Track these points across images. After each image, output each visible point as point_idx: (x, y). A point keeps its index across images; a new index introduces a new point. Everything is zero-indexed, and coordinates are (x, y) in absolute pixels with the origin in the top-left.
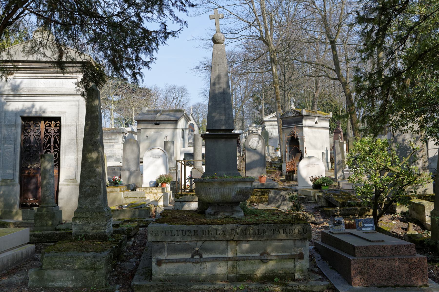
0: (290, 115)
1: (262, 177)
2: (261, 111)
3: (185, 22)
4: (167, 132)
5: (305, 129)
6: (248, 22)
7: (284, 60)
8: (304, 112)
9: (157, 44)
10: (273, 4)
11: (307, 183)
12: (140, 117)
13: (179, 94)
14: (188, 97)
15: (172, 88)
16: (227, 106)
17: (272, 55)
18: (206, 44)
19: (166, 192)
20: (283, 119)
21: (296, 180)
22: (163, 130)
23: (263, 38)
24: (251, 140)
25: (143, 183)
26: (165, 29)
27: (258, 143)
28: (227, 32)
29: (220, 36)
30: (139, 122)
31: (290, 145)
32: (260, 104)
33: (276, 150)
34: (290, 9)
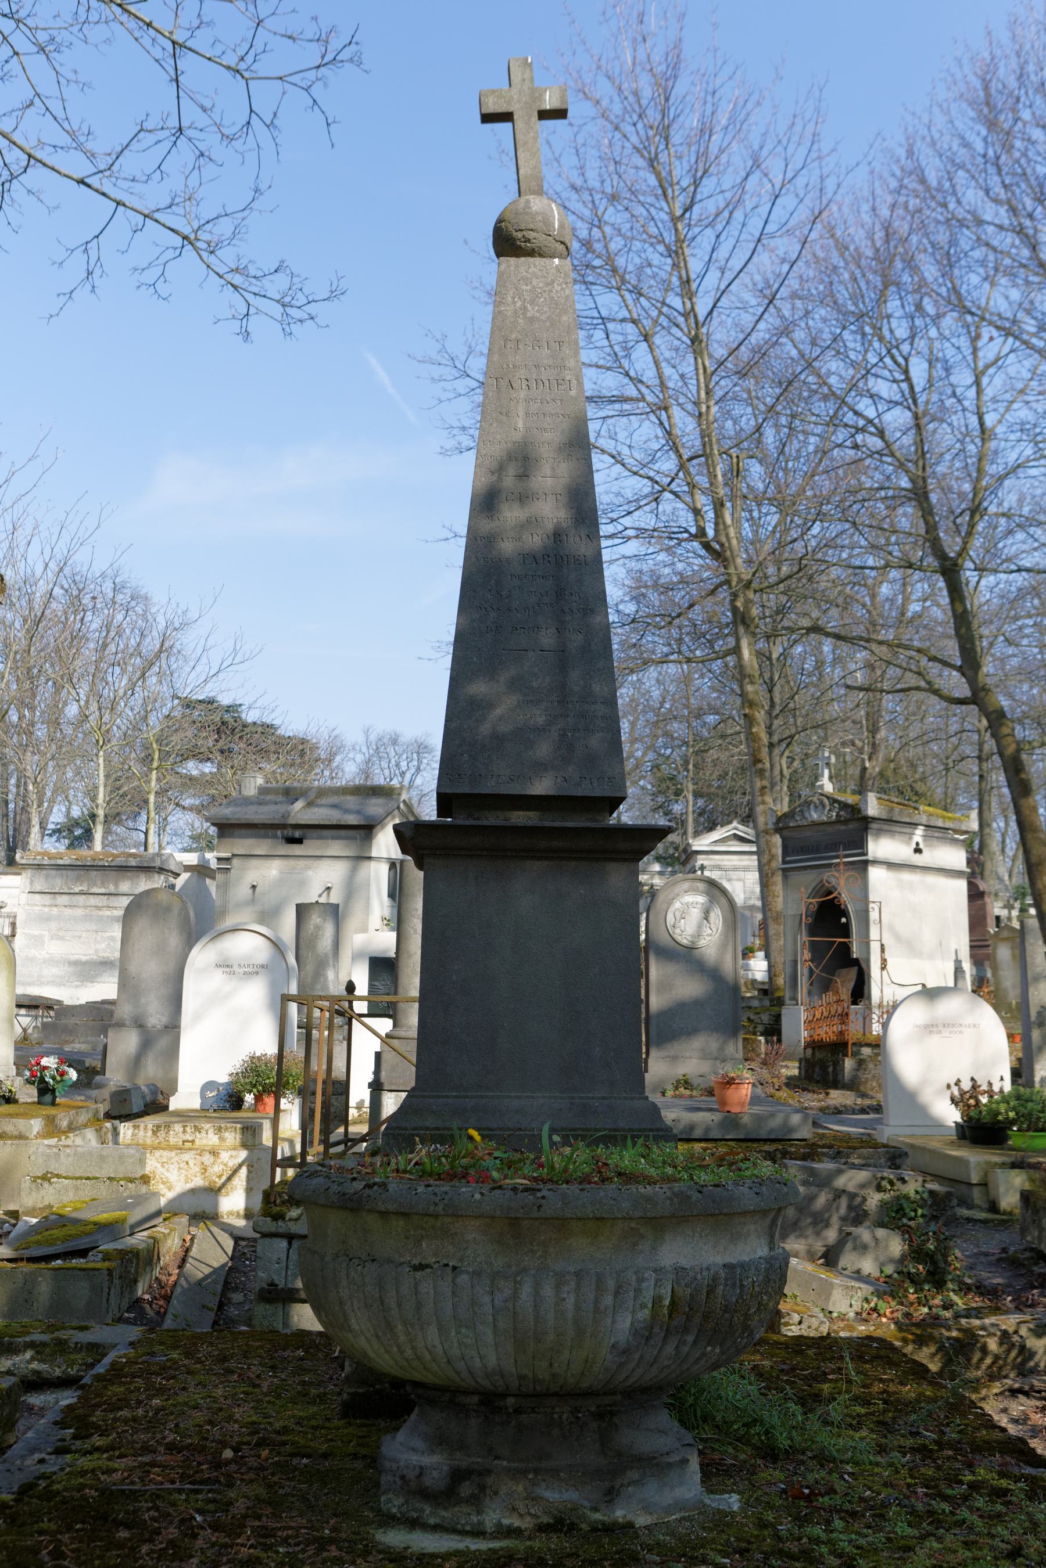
0: (815, 816)
1: (730, 1082)
4: (323, 875)
5: (875, 874)
8: (873, 807)
11: (922, 1111)
13: (409, 760)
15: (385, 740)
20: (786, 833)
24: (677, 905)
25: (174, 1090)
27: (706, 918)
31: (812, 932)
32: (678, 793)
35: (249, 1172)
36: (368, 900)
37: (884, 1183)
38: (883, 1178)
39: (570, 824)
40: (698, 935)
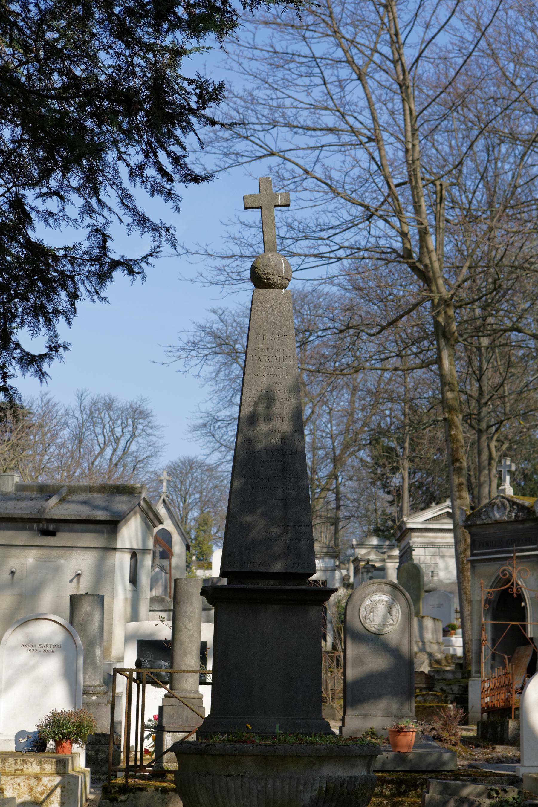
0: (497, 516)
1: (399, 731)
2: (398, 494)
3: (167, 230)
4: (77, 563)
6: (362, 205)
7: (479, 331)
9: (73, 296)
10: (446, 149)
13: (124, 426)
14: (153, 439)
15: (100, 405)
16: (293, 493)
17: (438, 313)
18: (220, 270)
19: (70, 771)
20: (474, 530)
21: (515, 742)
22: (68, 552)
23: (411, 257)
24: (368, 602)
26: (104, 248)
28: (292, 234)
29: (276, 262)
32: (395, 470)
33: (448, 631)
34: (499, 165)
35: (62, 791)
36: (113, 584)
37: (493, 793)
38: (492, 790)
39: (289, 587)
40: (384, 624)
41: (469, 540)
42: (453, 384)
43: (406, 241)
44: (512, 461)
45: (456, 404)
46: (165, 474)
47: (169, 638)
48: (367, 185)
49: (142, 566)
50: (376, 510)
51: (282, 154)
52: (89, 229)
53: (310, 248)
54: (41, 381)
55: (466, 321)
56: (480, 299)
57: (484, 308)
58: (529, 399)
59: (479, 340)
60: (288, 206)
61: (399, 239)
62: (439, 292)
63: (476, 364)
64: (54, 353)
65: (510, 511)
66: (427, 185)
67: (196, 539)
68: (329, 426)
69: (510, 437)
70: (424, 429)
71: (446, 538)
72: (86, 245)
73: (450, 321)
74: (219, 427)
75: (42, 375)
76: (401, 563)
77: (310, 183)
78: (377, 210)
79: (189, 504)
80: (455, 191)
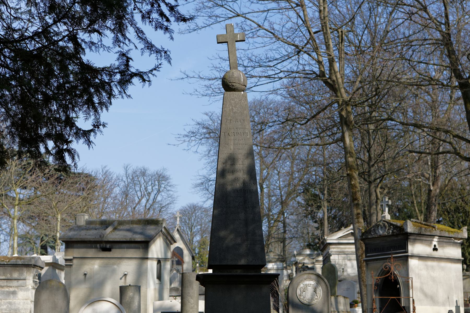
0: (381, 232)
2: (322, 224)
3: (166, 52)
5: (413, 262)
6: (293, 45)
7: (368, 120)
8: (410, 227)
10: (345, 10)
12: (71, 234)
14: (171, 193)
18: (208, 87)
20: (367, 241)
22: (118, 261)
23: (324, 76)
24: (302, 285)
26: (127, 65)
28: (252, 64)
29: (238, 75)
30: (70, 244)
31: (381, 294)
32: (319, 207)
34: (378, 19)
39: (250, 274)
40: (312, 299)
41: (364, 248)
42: (352, 153)
43: (321, 66)
44: (389, 199)
45: (354, 165)
46: (178, 213)
47: (180, 310)
48: (296, 33)
49: (165, 268)
50: (308, 233)
51: (244, 15)
52: (118, 54)
53: (263, 72)
54: (89, 146)
55: (359, 115)
56: (367, 100)
57: (370, 106)
58: (400, 162)
59: (368, 126)
60: (244, 41)
61: (318, 66)
62: (342, 97)
63: (367, 142)
64: (96, 129)
65: (388, 229)
66: (332, 32)
67: (199, 254)
68: (278, 182)
69: (389, 186)
70: (335, 182)
71: (351, 248)
72: (117, 63)
73: (349, 114)
74: (211, 185)
75: (89, 142)
76: (324, 264)
77: (261, 32)
78: (303, 48)
79: (194, 232)
80: (351, 36)
